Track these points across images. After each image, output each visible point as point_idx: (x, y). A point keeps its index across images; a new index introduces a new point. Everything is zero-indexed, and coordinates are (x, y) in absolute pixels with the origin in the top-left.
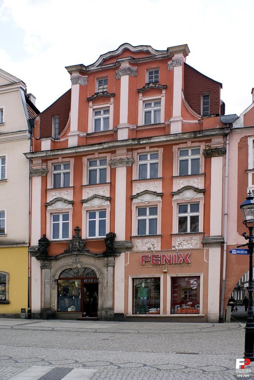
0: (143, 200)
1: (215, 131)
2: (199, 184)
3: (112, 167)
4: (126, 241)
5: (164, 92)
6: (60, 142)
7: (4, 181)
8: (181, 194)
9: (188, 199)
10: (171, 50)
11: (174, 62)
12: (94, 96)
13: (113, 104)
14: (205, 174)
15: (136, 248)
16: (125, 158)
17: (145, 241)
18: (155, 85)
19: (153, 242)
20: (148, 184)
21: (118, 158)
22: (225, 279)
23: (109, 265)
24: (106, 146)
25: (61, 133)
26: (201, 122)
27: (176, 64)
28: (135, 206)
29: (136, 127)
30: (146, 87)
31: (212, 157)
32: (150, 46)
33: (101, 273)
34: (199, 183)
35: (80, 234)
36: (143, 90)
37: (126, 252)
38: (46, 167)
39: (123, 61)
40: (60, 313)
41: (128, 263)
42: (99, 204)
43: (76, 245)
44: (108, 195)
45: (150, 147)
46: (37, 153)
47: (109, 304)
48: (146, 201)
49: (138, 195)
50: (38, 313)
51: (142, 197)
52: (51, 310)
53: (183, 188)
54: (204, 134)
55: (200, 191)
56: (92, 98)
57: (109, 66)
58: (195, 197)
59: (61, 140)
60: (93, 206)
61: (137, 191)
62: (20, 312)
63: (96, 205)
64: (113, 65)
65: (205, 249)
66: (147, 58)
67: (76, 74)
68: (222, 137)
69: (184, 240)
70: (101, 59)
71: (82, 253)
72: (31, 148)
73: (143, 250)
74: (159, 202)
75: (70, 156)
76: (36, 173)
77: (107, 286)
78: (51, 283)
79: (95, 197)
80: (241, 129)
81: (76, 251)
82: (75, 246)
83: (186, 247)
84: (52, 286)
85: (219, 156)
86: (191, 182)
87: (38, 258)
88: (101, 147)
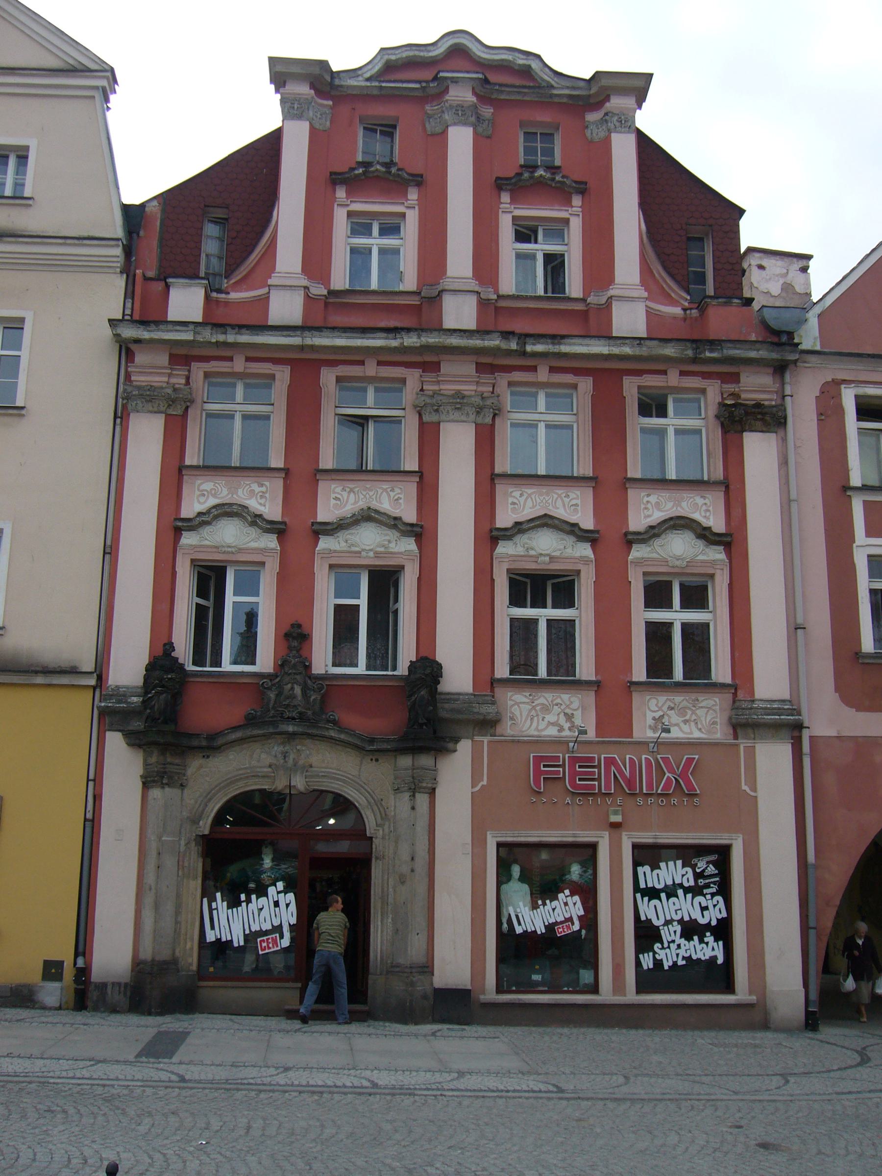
0: (532, 549)
1: (758, 350)
2: (708, 514)
3: (426, 418)
4: (475, 695)
5: (577, 201)
6: (227, 303)
7: (11, 411)
8: (657, 542)
9: (678, 563)
10: (604, 82)
11: (612, 117)
12: (356, 172)
13: (417, 207)
14: (420, 473)
15: (509, 723)
16: (473, 393)
17: (542, 700)
18: (553, 174)
19: (568, 706)
20: (548, 494)
21: (449, 388)
22: (813, 861)
23: (421, 788)
24: (410, 340)
25: (233, 271)
26: (691, 314)
27: (618, 124)
28: (505, 566)
29: (495, 297)
30: (525, 175)
31: (745, 431)
32: (538, 57)
33: (382, 818)
34: (709, 511)
35: (304, 653)
36: (515, 184)
37: (477, 738)
38: (183, 381)
39: (455, 81)
40: (211, 983)
41: (485, 782)
42: (377, 546)
43: (294, 697)
44: (410, 515)
45: (552, 370)
46: (161, 327)
47: (415, 951)
48: (541, 554)
49: (519, 528)
50: (119, 984)
51: (530, 539)
52: (178, 971)
53: (665, 521)
54: (725, 351)
55: (717, 539)
56: (347, 176)
57: (405, 85)
58: (701, 557)
59: (234, 296)
60: (357, 549)
61: (510, 513)
62: (33, 974)
63: (368, 548)
64: (417, 86)
65: (743, 744)
66: (524, 87)
67: (304, 90)
68: (770, 370)
69: (673, 705)
70: (381, 58)
71: (319, 732)
72: (129, 305)
73: (536, 733)
74: (584, 560)
75: (275, 355)
76: (147, 401)
77: (412, 871)
78: (182, 848)
79: (368, 516)
80: (823, 357)
81: (293, 719)
82: (288, 698)
83: (681, 735)
84: (186, 864)
85: (764, 429)
86: (684, 504)
87: (135, 740)
88: (394, 343)
